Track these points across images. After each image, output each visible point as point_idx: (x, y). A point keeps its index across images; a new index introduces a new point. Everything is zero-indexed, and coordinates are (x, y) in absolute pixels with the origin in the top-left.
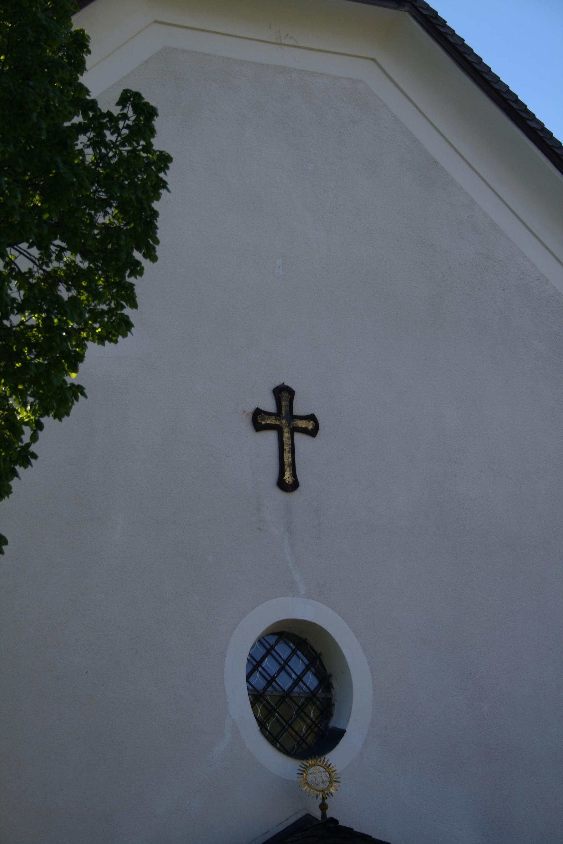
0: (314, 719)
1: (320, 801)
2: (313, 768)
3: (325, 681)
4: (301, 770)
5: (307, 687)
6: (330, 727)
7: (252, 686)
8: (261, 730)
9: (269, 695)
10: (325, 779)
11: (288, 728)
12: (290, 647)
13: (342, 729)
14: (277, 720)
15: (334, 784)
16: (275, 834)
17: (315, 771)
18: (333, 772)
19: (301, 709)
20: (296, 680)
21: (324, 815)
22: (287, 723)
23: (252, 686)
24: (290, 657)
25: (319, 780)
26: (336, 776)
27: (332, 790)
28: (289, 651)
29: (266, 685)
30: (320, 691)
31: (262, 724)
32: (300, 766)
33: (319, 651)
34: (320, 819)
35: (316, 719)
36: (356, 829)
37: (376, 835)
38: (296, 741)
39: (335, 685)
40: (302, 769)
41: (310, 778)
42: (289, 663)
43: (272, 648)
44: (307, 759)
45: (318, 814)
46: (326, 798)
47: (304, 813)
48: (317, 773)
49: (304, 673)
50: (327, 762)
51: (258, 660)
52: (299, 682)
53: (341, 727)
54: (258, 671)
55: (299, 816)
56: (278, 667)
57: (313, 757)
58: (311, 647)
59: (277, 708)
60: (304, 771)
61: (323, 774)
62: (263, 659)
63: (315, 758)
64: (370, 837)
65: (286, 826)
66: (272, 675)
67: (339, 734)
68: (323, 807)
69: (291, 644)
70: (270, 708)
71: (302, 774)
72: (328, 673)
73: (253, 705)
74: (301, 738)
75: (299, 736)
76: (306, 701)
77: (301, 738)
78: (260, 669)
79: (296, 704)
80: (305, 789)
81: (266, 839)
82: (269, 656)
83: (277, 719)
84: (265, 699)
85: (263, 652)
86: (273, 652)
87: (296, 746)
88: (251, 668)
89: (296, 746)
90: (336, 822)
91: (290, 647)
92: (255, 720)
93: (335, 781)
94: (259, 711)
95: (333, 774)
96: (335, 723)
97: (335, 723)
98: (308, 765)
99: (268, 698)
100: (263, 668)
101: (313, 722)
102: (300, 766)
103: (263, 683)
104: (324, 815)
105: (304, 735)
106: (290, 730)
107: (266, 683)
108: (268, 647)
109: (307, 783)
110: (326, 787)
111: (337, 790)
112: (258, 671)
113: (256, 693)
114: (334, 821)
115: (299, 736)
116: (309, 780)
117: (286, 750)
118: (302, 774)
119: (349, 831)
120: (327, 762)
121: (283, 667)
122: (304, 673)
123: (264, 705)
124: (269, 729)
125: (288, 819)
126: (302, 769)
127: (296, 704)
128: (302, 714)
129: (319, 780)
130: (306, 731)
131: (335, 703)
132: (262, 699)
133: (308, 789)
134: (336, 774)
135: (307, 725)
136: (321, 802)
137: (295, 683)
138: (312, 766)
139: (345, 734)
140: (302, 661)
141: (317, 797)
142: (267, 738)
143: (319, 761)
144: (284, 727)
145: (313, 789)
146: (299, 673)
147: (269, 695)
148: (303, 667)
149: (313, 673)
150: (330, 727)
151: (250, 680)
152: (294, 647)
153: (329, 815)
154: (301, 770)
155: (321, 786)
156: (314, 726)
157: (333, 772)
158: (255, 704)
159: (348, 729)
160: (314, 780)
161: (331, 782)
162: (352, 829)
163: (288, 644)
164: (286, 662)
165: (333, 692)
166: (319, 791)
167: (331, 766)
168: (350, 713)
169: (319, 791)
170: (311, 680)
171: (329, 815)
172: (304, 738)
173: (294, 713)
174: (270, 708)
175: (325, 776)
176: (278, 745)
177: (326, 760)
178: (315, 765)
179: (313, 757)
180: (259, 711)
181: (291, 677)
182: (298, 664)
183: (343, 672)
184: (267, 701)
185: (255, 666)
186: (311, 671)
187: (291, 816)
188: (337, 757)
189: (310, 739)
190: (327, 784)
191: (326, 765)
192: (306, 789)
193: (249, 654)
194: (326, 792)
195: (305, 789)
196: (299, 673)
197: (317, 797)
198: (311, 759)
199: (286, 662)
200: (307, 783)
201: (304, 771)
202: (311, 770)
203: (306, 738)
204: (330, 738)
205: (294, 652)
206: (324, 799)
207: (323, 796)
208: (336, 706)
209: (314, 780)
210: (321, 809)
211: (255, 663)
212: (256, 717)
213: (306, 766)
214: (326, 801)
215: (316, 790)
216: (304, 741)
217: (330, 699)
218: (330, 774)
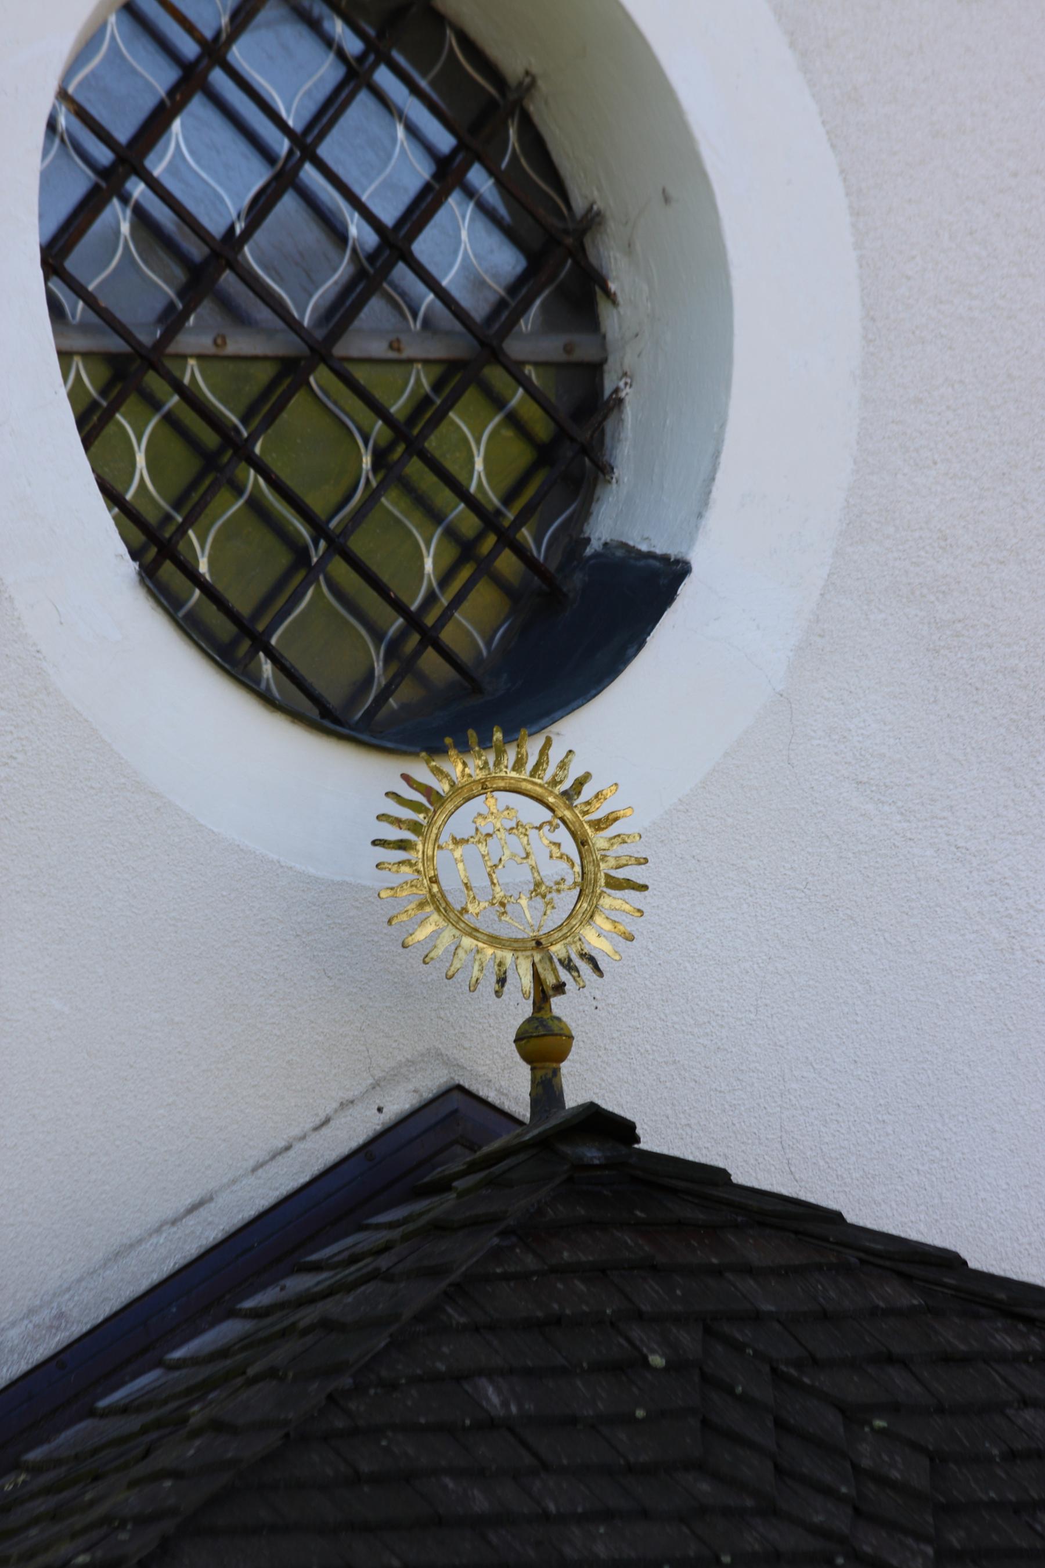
0: (493, 499)
1: (519, 1009)
2: (477, 804)
3: (562, 257)
4: (397, 822)
5: (443, 295)
6: (595, 546)
7: (90, 301)
8: (150, 577)
9: (200, 357)
10: (553, 870)
11: (324, 559)
12: (328, 42)
13: (665, 559)
14: (256, 506)
15: (612, 900)
16: (250, 1212)
17: (485, 827)
18: (598, 825)
19: (408, 439)
20: (372, 257)
21: (546, 1091)
22: (319, 529)
23: (90, 301)
24: (329, 111)
25: (515, 876)
26: (618, 850)
27: (595, 939)
28: (326, 73)
29: (171, 93)
30: (527, 324)
31: (156, 552)
32: (392, 795)
33: (514, 64)
34: (522, 1110)
35: (508, 499)
36: (752, 1170)
37: (879, 1206)
38: (378, 636)
39: (621, 275)
40: (406, 814)
41: (456, 867)
42: (324, 151)
43: (215, 51)
44: (436, 750)
45: (510, 1086)
46: (560, 988)
47: (429, 1082)
48: (496, 829)
49: (423, 208)
50: (563, 765)
51: (123, 135)
52: (390, 266)
53: (652, 538)
54: (125, 199)
55: (399, 1102)
56: (256, 176)
57: (472, 735)
58: (466, 41)
59: (253, 438)
60: (415, 827)
61: (540, 843)
62: (155, 126)
63: (485, 742)
64: (835, 1217)
65: (316, 1167)
66: (208, 34)
67: (647, 587)
68: (542, 1043)
69: (338, 28)
70: (210, 439)
71: (402, 845)
72: (579, 205)
73: (92, 423)
74: (413, 621)
75: (400, 607)
76: (438, 386)
77: (413, 621)
78: (138, 189)
79: (379, 411)
80: (422, 934)
81: (192, 1249)
82: (198, 106)
83: (256, 506)
84: (178, 387)
85: (158, 78)
86: (218, 77)
87: (378, 667)
88: (78, 182)
89: (378, 667)
90: (622, 1130)
91: (328, 42)
92: (101, 519)
93: (615, 884)
94: (141, 459)
95: (599, 840)
96: (619, 519)
97: (619, 519)
98: (443, 787)
99: (192, 372)
100: (154, 185)
101: (489, 519)
102: (392, 795)
103: (161, 285)
104: (546, 1091)
105: (431, 598)
106: (339, 568)
107: (180, 274)
108: (190, 49)
109: (438, 902)
110: (558, 916)
111: (630, 938)
112: (125, 199)
113: (115, 344)
114: (610, 1128)
115: (400, 607)
116: (450, 883)
117: (326, 712)
118: (402, 845)
119: (705, 1182)
120: (563, 765)
121: (292, 164)
122: (423, 208)
123: (170, 420)
124: (203, 568)
125: (327, 1121)
126: (406, 814)
127: (379, 411)
128: (415, 468)
129: (515, 876)
130: (444, 581)
131: (626, 393)
132: (153, 381)
133: (448, 935)
134: (621, 839)
135: (451, 533)
136: (527, 1010)
137: (370, 277)
138: (464, 793)
139: (686, 589)
140: (412, 130)
141: (502, 981)
142: (191, 628)
143: (511, 756)
144: (301, 555)
145: (473, 932)
146: (388, 216)
147: (200, 357)
148: (422, 171)
149: (484, 208)
150: (595, 546)
151: (72, 264)
152: (353, 46)
153: (578, 1088)
154: (397, 822)
155: (528, 917)
156: (491, 540)
157: (598, 825)
158: (108, 416)
159: (705, 558)
160: (480, 881)
161: (585, 887)
162: (721, 1176)
163: (314, 25)
164: (306, 144)
165: (614, 321)
166: (516, 945)
167: (588, 792)
168: (717, 455)
169: (516, 945)
170: (467, 250)
171: (574, 1097)
172: (430, 620)
173: (367, 461)
174: (210, 439)
175: (551, 854)
176: (267, 668)
177: (556, 755)
178: (485, 787)
179: (472, 735)
180: (141, 459)
181: (339, 235)
182: (383, 157)
183: (667, 199)
184: (190, 397)
185: (103, 173)
186: (470, 193)
187: (346, 1105)
188: (619, 737)
189: (474, 626)
190: (566, 900)
191: (554, 782)
192: (436, 934)
193: (63, 95)
194: (558, 950)
195: (422, 934)
196: (388, 216)
197: (502, 981)
198: (464, 748)
199: (306, 144)
200: (438, 902)
201: (415, 827)
202: (461, 820)
203: (446, 616)
204: (588, 615)
205: (355, 76)
206: (543, 994)
207: (536, 977)
208: (629, 412)
209: (480, 881)
210: (528, 1057)
211: (104, 156)
212: (111, 495)
213: (427, 791)
214: (558, 1005)
215: (494, 941)
216: (430, 639)
217: (595, 370)
218: (582, 843)
